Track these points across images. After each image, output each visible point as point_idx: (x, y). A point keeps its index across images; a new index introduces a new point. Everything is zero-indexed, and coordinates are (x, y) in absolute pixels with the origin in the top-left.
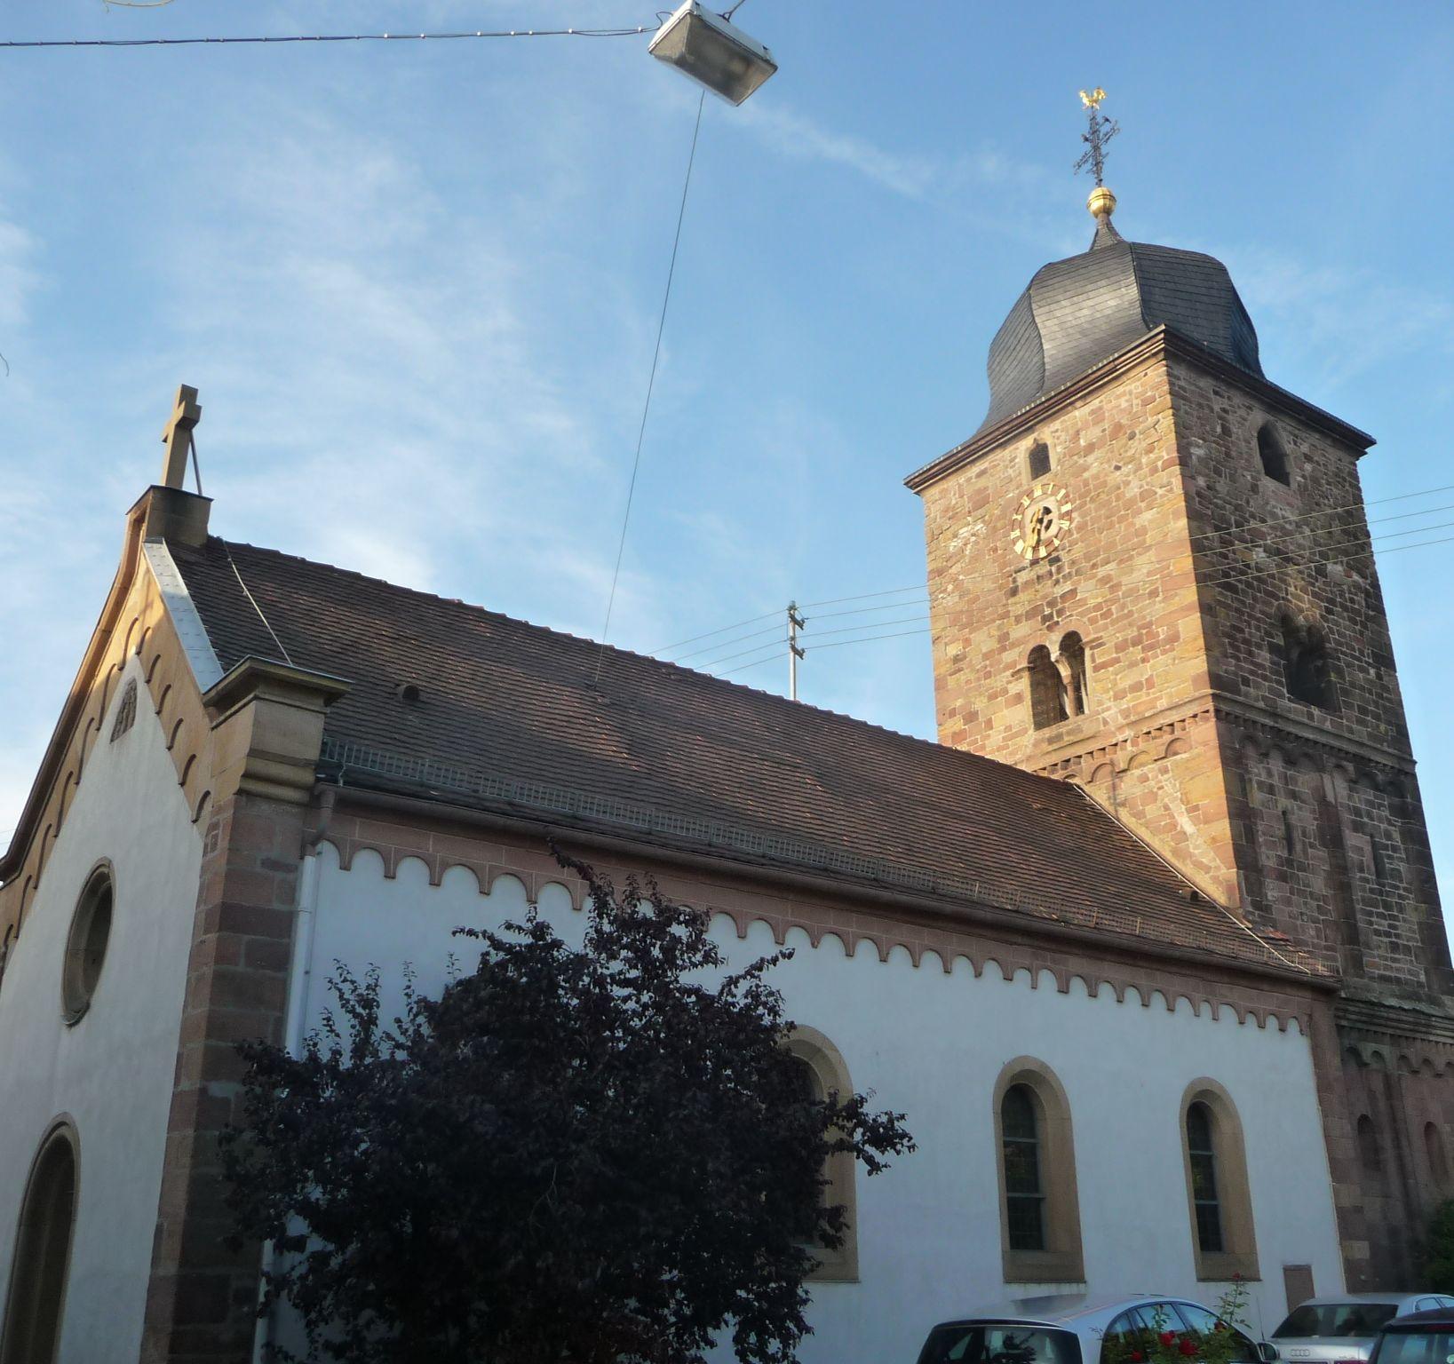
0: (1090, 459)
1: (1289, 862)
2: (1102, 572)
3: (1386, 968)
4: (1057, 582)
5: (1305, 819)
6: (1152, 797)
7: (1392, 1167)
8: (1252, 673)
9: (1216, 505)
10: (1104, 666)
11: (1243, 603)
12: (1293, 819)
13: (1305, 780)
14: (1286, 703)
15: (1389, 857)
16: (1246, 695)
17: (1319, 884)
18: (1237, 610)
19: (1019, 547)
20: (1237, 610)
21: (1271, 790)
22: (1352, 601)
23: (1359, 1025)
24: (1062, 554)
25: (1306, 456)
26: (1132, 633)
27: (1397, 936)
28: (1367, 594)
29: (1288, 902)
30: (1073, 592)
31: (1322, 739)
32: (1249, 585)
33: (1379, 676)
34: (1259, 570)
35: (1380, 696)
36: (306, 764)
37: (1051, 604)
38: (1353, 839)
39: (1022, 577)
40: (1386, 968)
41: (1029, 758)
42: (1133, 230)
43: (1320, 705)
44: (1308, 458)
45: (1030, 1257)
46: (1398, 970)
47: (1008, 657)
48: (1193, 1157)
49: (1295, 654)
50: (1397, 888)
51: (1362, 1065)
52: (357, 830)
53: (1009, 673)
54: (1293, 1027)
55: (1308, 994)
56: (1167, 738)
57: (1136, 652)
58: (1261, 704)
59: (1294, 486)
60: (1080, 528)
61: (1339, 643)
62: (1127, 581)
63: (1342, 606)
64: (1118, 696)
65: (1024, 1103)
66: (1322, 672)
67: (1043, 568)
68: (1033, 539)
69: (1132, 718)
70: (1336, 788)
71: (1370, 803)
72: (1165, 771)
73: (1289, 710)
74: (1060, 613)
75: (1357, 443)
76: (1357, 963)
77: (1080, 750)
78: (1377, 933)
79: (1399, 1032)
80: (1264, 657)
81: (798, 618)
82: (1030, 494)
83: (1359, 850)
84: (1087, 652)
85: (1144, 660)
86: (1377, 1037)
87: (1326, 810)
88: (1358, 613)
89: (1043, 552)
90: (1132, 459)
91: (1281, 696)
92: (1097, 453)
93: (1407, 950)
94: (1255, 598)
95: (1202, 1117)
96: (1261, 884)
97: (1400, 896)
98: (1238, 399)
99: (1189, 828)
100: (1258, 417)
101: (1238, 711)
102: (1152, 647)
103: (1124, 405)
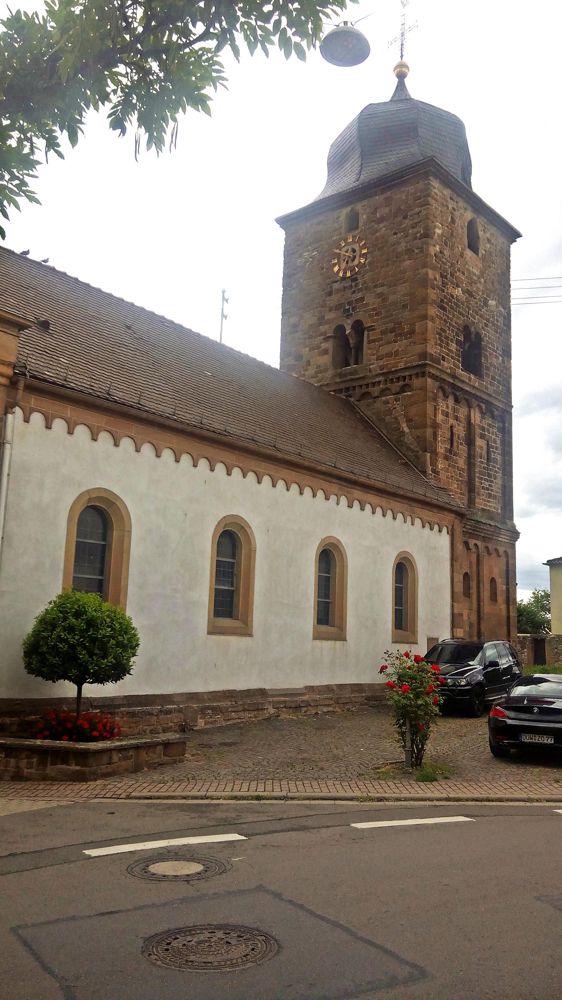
0: (381, 225)
1: (450, 451)
2: (379, 290)
3: (485, 505)
4: (354, 292)
5: (460, 431)
6: (389, 412)
7: (474, 597)
8: (448, 355)
9: (443, 262)
10: (374, 341)
11: (448, 317)
12: (455, 430)
13: (462, 412)
14: (460, 372)
15: (494, 452)
16: (443, 365)
17: (462, 463)
18: (445, 320)
19: (336, 269)
20: (445, 320)
21: (447, 415)
22: (497, 321)
23: (470, 531)
24: (359, 277)
25: (488, 239)
26: (391, 325)
27: (492, 490)
28: (505, 317)
29: (447, 471)
30: (362, 299)
31: (473, 391)
32: (452, 308)
33: (503, 362)
34: (457, 299)
35: (502, 371)
36: (9, 364)
37: (349, 303)
38: (480, 443)
39: (336, 286)
40: (485, 505)
41: (327, 385)
42: (417, 91)
43: (475, 375)
44: (489, 240)
45: (225, 622)
46: (490, 506)
47: (323, 328)
48: (219, 564)
49: (467, 345)
50: (495, 467)
51: (468, 549)
52: (33, 400)
53: (322, 337)
54: (445, 530)
55: (453, 516)
56: (401, 383)
57: (391, 336)
58: (449, 371)
59: (480, 255)
60: (370, 264)
61: (487, 341)
62: (391, 298)
63: (492, 323)
64: (379, 358)
65: (232, 542)
66: (479, 356)
67: (347, 284)
68: (344, 265)
69: (385, 371)
70: (476, 417)
71: (489, 425)
72: (396, 400)
73: (461, 375)
74: (354, 309)
75: (514, 235)
76: (471, 502)
77: (355, 384)
78: (483, 488)
79: (486, 535)
80: (453, 346)
81: (226, 297)
82: (346, 240)
83: (482, 448)
84: (366, 333)
85: (395, 341)
86: (476, 537)
87: (469, 425)
88: (499, 327)
89: (348, 274)
90: (404, 230)
91: (458, 368)
92: (384, 223)
93: (495, 497)
94: (453, 315)
95: (403, 569)
96: (437, 460)
97: (496, 472)
98: (462, 204)
99: (406, 430)
100: (469, 215)
101: (438, 374)
102: (400, 335)
103: (404, 198)
